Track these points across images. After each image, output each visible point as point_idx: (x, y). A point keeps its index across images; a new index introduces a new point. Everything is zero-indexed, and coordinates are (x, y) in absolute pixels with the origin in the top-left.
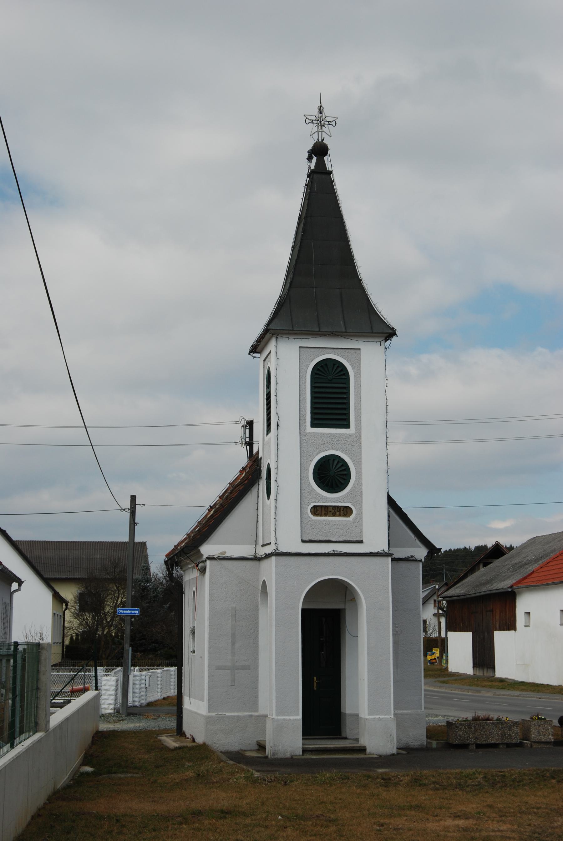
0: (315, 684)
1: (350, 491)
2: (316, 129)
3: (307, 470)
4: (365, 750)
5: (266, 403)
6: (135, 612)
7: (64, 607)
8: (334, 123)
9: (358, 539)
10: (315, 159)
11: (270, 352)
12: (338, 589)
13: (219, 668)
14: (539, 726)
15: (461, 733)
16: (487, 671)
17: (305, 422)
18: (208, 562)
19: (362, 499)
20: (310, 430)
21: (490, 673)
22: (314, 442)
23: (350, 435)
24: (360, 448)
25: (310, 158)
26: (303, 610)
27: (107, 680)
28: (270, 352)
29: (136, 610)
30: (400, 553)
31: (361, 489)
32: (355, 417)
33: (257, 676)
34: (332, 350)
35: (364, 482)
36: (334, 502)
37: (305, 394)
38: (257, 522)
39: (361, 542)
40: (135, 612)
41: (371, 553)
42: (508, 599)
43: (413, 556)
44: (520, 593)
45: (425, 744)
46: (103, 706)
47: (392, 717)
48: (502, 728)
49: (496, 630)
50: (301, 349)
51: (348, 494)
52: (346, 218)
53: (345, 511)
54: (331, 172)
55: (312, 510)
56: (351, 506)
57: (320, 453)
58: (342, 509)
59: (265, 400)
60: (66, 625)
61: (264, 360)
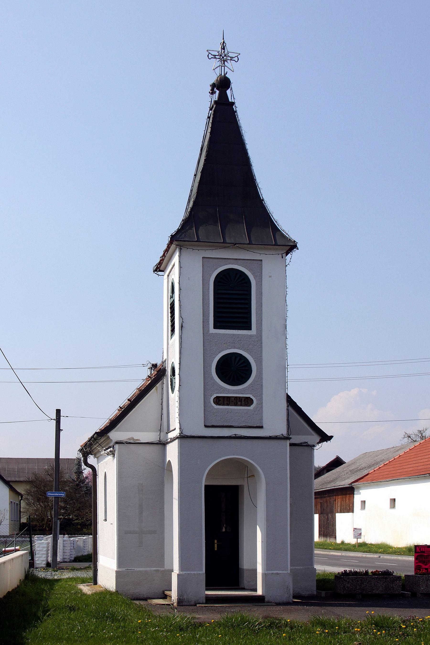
0: (216, 545)
1: (251, 384)
2: (219, 64)
3: (211, 366)
4: (264, 599)
5: (169, 311)
6: (62, 494)
7: (20, 498)
8: (236, 59)
9: (258, 425)
10: (218, 92)
11: (174, 265)
12: (241, 467)
13: (127, 533)
14: (427, 581)
15: (349, 585)
16: (330, 539)
17: (209, 324)
18: (117, 446)
19: (262, 392)
20: (212, 330)
21: (332, 540)
22: (216, 342)
23: (251, 336)
24: (261, 347)
25: (213, 93)
26: (206, 486)
27: (39, 544)
28: (174, 265)
29: (62, 493)
30: (296, 439)
31: (262, 382)
32: (257, 321)
33: (164, 539)
34: (234, 261)
35: (264, 376)
36: (236, 393)
37: (209, 299)
38: (162, 414)
39: (262, 427)
40: (62, 494)
41: (270, 437)
42: (349, 491)
43: (306, 443)
44: (359, 488)
45: (315, 593)
46: (38, 562)
47: (289, 572)
48: (386, 581)
49: (338, 512)
50: (205, 259)
51: (249, 386)
52: (248, 147)
53: (248, 402)
54: (233, 103)
55: (215, 400)
56: (252, 397)
57: (222, 351)
58: (243, 400)
59: (169, 309)
60: (21, 510)
61: (146, 599)
